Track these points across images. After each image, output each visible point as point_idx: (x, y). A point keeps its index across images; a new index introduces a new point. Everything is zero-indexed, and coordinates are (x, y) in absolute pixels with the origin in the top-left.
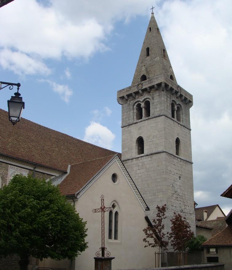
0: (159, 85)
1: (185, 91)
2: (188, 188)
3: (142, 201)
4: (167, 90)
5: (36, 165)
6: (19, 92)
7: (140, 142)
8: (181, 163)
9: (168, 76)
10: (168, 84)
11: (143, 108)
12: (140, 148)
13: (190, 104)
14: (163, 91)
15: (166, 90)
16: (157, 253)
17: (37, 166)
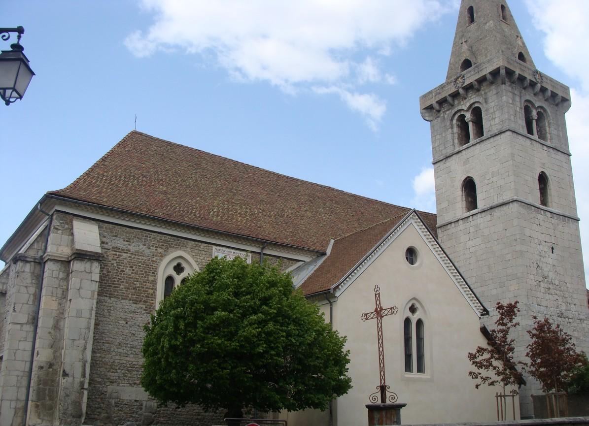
0: (495, 73)
1: (552, 80)
2: (572, 269)
3: (473, 297)
4: (513, 80)
5: (265, 242)
6: (21, 43)
7: (469, 186)
8: (553, 221)
9: (514, 55)
10: (512, 69)
11: (470, 121)
12: (470, 200)
13: (565, 104)
14: (504, 83)
15: (510, 81)
16: (499, 394)
17: (267, 246)
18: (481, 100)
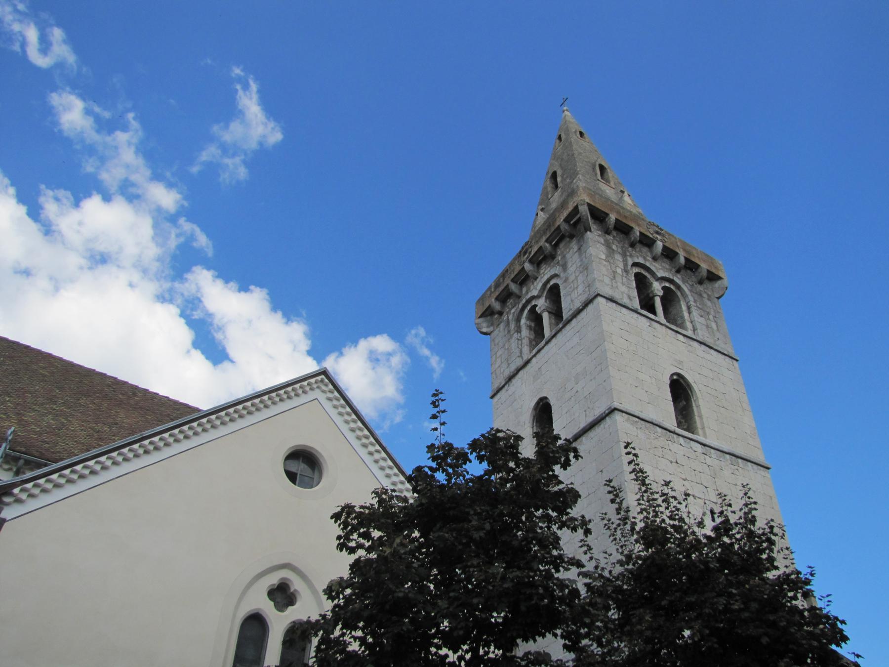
18: (556, 270)
